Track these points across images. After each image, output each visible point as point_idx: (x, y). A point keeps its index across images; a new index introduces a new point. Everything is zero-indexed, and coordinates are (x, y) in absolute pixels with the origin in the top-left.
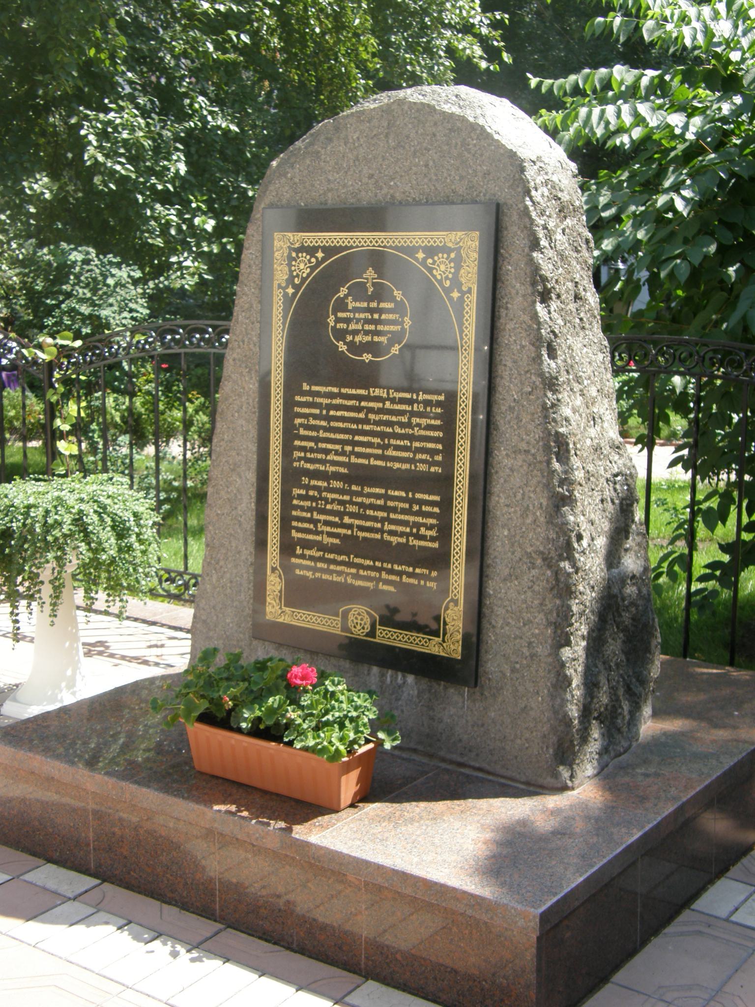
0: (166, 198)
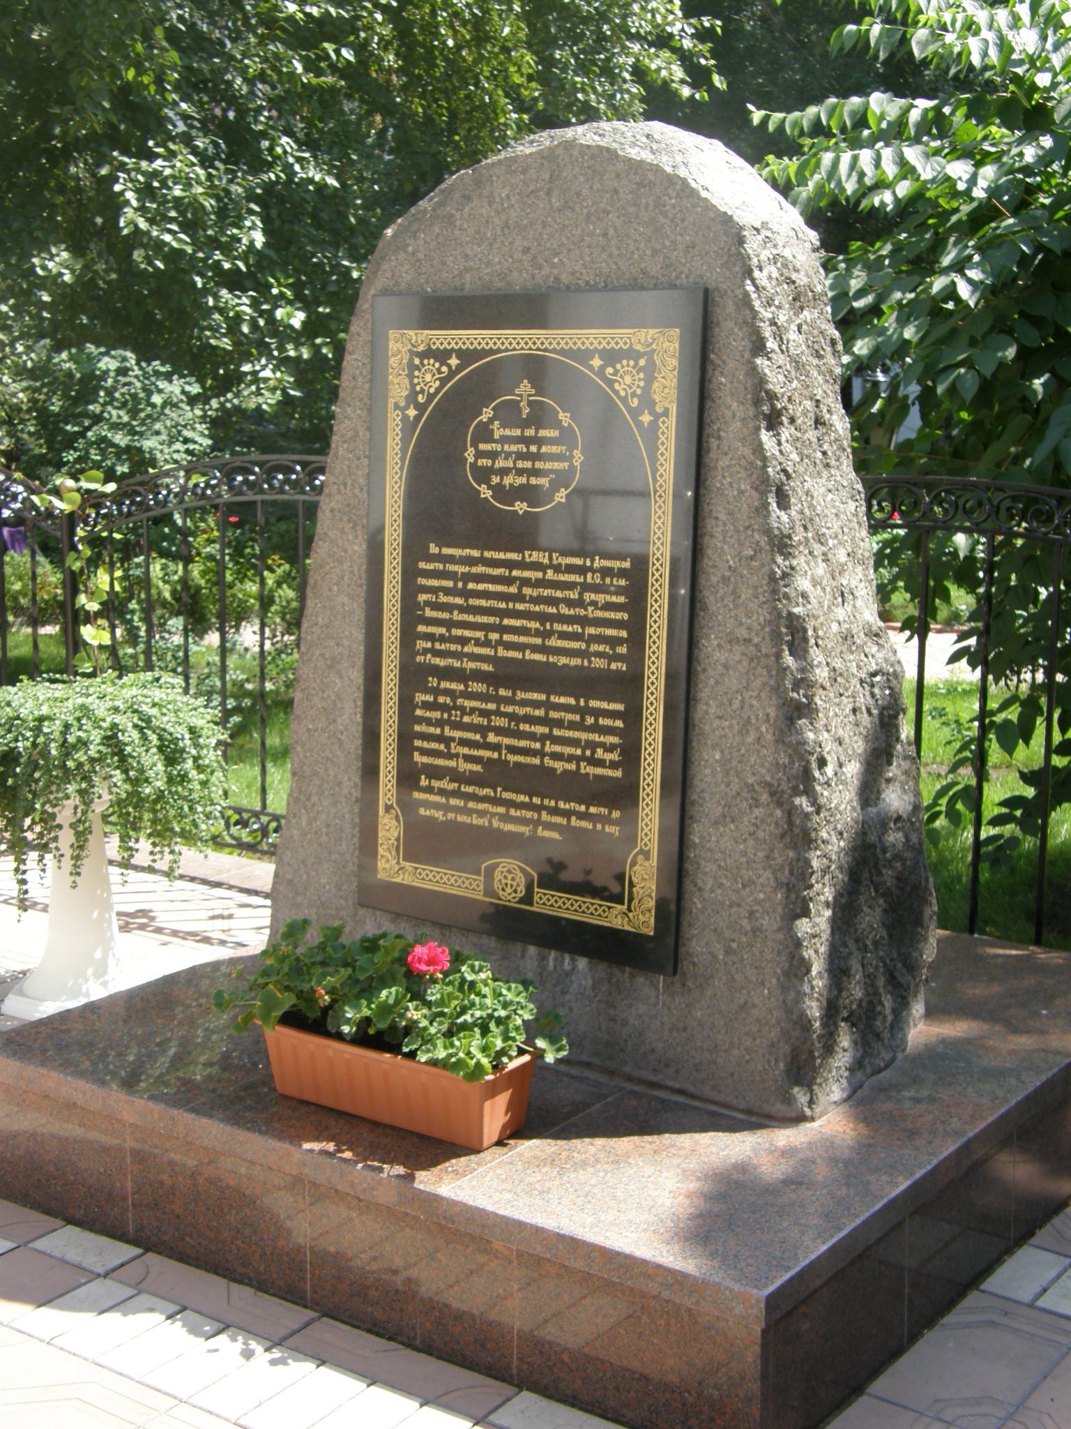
0: (235, 282)
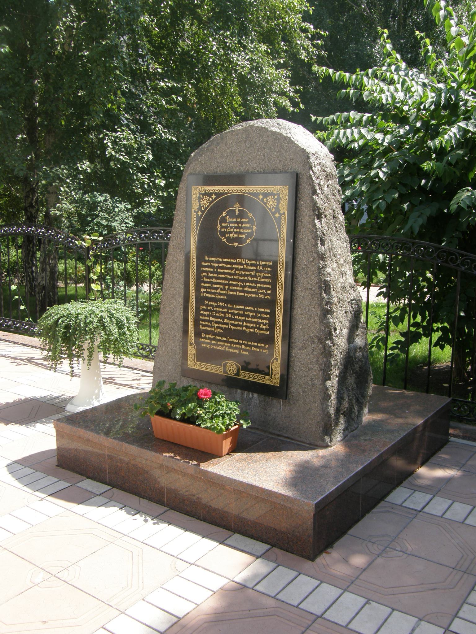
0: (143, 171)
